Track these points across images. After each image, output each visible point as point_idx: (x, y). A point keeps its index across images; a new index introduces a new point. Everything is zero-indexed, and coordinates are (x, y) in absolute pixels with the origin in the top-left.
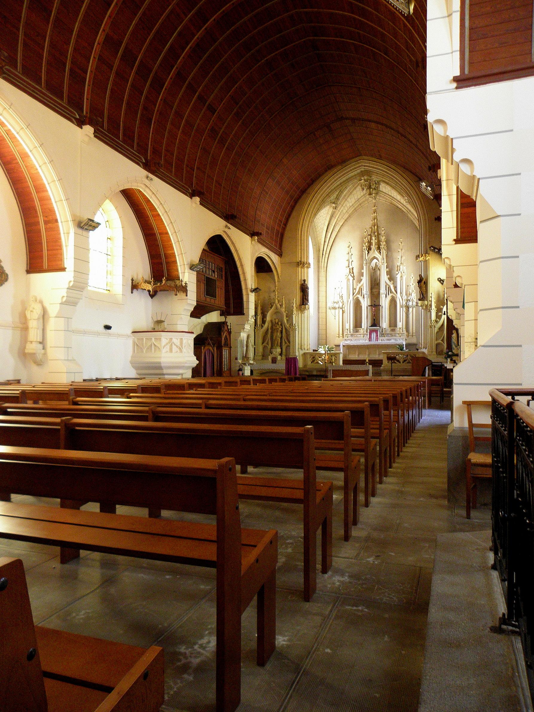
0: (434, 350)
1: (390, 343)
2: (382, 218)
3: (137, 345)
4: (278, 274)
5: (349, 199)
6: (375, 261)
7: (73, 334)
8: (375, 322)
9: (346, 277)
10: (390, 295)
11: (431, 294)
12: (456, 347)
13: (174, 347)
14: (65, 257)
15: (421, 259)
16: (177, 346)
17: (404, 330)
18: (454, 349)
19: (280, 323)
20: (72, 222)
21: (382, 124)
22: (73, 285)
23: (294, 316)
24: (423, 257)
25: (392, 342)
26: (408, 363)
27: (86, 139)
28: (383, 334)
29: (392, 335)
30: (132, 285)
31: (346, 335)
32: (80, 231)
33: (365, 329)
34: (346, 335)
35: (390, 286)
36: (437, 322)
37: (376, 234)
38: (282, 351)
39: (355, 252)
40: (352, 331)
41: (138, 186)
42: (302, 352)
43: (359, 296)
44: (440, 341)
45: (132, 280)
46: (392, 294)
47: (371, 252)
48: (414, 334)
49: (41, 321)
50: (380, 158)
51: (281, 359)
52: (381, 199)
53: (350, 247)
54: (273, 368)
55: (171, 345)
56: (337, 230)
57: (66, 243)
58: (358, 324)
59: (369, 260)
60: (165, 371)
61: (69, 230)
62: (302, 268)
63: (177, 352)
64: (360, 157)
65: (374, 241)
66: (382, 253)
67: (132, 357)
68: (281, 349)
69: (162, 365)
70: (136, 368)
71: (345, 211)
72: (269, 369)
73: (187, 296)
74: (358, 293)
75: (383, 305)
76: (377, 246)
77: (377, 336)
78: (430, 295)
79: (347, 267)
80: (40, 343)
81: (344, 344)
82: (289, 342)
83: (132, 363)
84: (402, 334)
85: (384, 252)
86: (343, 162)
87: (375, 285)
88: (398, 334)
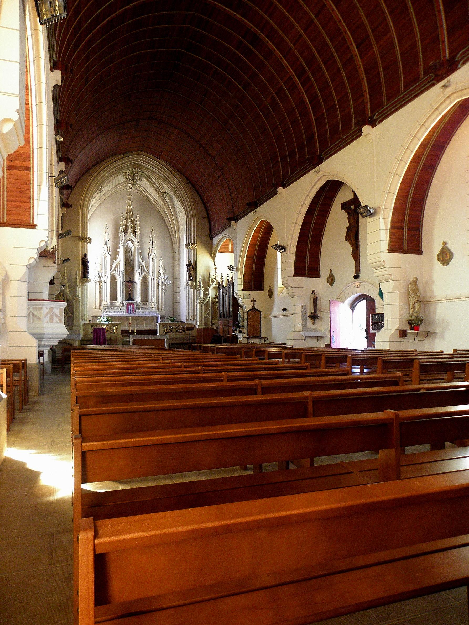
8: (129, 297)
10: (144, 273)
11: (200, 276)
12: (242, 320)
13: (55, 317)
16: (57, 316)
17: (155, 304)
19: (62, 294)
24: (192, 246)
25: (147, 314)
28: (137, 307)
29: (145, 309)
33: (122, 302)
35: (143, 266)
36: (204, 299)
40: (109, 303)
43: (116, 272)
46: (144, 273)
47: (127, 234)
50: (159, 157)
58: (113, 298)
59: (126, 240)
64: (141, 152)
65: (130, 225)
74: (115, 270)
75: (137, 282)
77: (134, 309)
78: (198, 277)
82: (73, 314)
84: (154, 307)
86: (125, 152)
87: (129, 263)
88: (151, 307)
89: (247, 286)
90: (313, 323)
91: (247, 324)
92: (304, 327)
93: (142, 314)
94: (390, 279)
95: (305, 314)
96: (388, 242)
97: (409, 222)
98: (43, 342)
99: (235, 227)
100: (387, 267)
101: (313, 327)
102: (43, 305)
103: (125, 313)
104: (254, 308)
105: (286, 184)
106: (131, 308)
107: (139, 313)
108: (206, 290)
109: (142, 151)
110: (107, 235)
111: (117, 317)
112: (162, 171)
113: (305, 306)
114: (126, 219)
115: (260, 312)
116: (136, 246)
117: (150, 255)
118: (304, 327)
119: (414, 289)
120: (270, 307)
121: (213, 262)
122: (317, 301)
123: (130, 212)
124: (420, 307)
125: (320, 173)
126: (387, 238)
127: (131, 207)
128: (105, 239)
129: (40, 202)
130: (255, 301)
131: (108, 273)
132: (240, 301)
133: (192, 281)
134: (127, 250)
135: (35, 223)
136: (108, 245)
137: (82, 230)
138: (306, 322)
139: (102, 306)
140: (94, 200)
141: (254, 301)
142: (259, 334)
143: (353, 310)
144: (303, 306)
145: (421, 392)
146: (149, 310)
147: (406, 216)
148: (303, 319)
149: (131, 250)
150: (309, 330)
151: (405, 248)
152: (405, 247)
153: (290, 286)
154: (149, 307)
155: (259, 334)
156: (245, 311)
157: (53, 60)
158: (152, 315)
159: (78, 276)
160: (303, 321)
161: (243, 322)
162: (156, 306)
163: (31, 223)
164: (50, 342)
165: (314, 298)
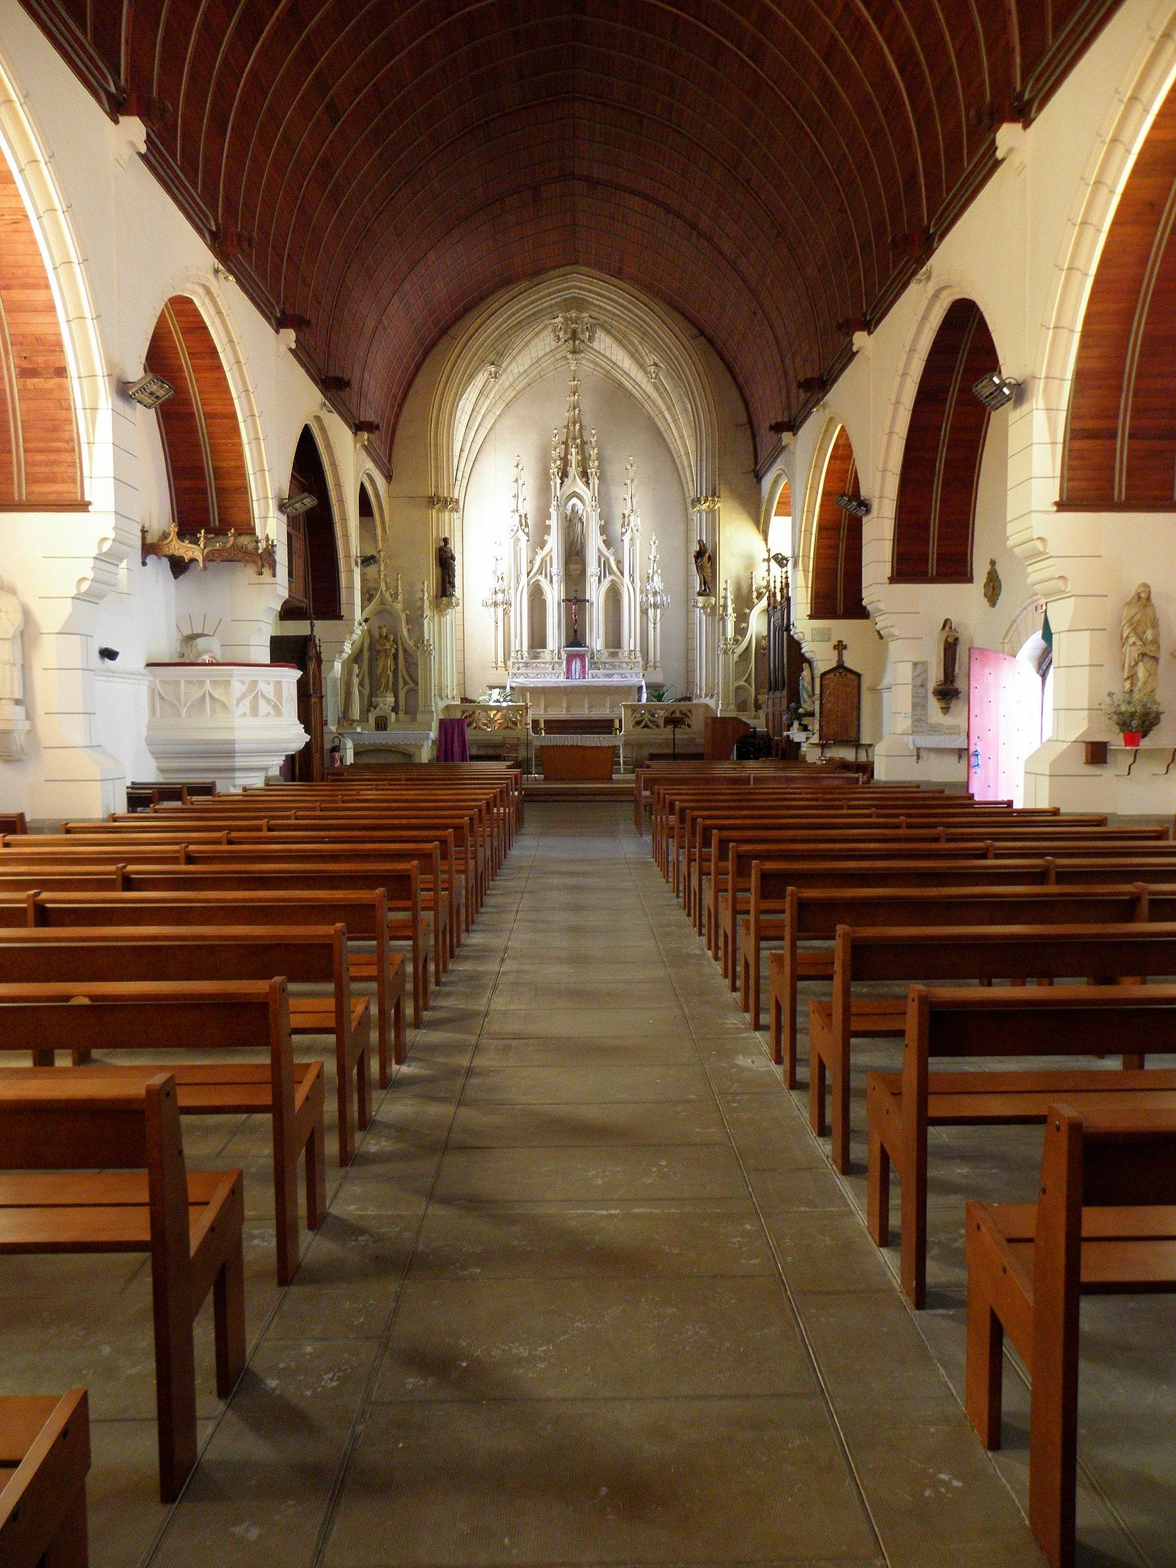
0: (732, 701)
1: (611, 684)
2: (588, 405)
3: (162, 698)
4: (383, 522)
5: (519, 359)
6: (575, 500)
7: (96, 678)
8: (575, 637)
9: (513, 533)
10: (609, 578)
11: (726, 582)
12: (809, 697)
13: (262, 702)
14: (86, 473)
15: (704, 507)
16: (268, 701)
17: (638, 654)
18: (805, 702)
20: (106, 378)
21: (657, 202)
22: (111, 549)
23: (426, 621)
24: (707, 504)
25: (616, 680)
26: (644, 727)
27: (127, 153)
28: (595, 663)
29: (614, 667)
30: (144, 545)
31: (514, 663)
32: (121, 406)
33: (556, 651)
34: (514, 663)
35: (608, 560)
36: (736, 642)
37: (578, 441)
38: (396, 702)
39: (529, 479)
40: (525, 654)
41: (193, 292)
42: (442, 704)
43: (541, 578)
44: (742, 683)
45: (144, 532)
47: (567, 481)
48: (658, 664)
49: (19, 642)
50: (618, 274)
51: (397, 720)
52: (585, 364)
53: (520, 467)
54: (384, 743)
55: (256, 697)
56: (488, 424)
57: (88, 435)
58: (538, 641)
59: (564, 497)
60: (239, 762)
61: (95, 399)
62: (439, 510)
63: (268, 714)
64: (576, 267)
65: (574, 457)
66: (591, 485)
67: (151, 727)
68: (396, 696)
69: (237, 747)
70: (157, 756)
71: (507, 384)
72: (374, 745)
73: (274, 575)
74: (540, 572)
75: (594, 599)
76: (580, 469)
77: (583, 667)
78: (722, 585)
79: (513, 511)
80: (18, 702)
81: (514, 685)
82: (416, 683)
83: (150, 742)
84: (635, 663)
85: (595, 481)
86: (535, 273)
87: (574, 553)
88: (627, 663)
89: (823, 608)
90: (946, 710)
91: (821, 708)
92: (918, 720)
93: (602, 681)
94: (1062, 592)
95: (922, 686)
96: (1058, 480)
97: (1137, 412)
98: (237, 760)
99: (792, 447)
100: (1051, 557)
101: (947, 720)
102: (231, 676)
103: (562, 679)
104: (840, 667)
105: (871, 320)
106: (576, 665)
107: (596, 678)
108: (742, 618)
109: (576, 263)
110: (520, 486)
111: (543, 688)
112: (630, 311)
113: (924, 663)
114: (565, 443)
115: (858, 676)
116: (589, 509)
117: (624, 530)
118: (919, 722)
119: (1136, 618)
120: (880, 661)
121: (763, 542)
122: (955, 651)
123: (574, 424)
124: (1152, 674)
125: (931, 284)
126: (1054, 467)
127: (577, 412)
128: (514, 496)
129: (95, 447)
130: (845, 647)
131: (524, 580)
132: (806, 649)
133: (707, 595)
134: (572, 523)
135: (87, 499)
136: (523, 512)
137: (437, 481)
138: (924, 707)
139: (510, 663)
140: (488, 402)
141: (840, 647)
142: (853, 735)
143: (1044, 676)
144: (915, 664)
145: (74, 1002)
146: (623, 669)
147: (1124, 396)
148: (916, 700)
149: (580, 519)
150: (934, 729)
151: (1120, 492)
152: (1120, 489)
153: (880, 610)
154: (622, 663)
155: (853, 735)
156: (818, 672)
157: (108, 94)
158: (627, 683)
159: (429, 593)
160: (914, 706)
161: (812, 703)
162: (639, 659)
163: (79, 499)
164: (249, 759)
165: (946, 640)
